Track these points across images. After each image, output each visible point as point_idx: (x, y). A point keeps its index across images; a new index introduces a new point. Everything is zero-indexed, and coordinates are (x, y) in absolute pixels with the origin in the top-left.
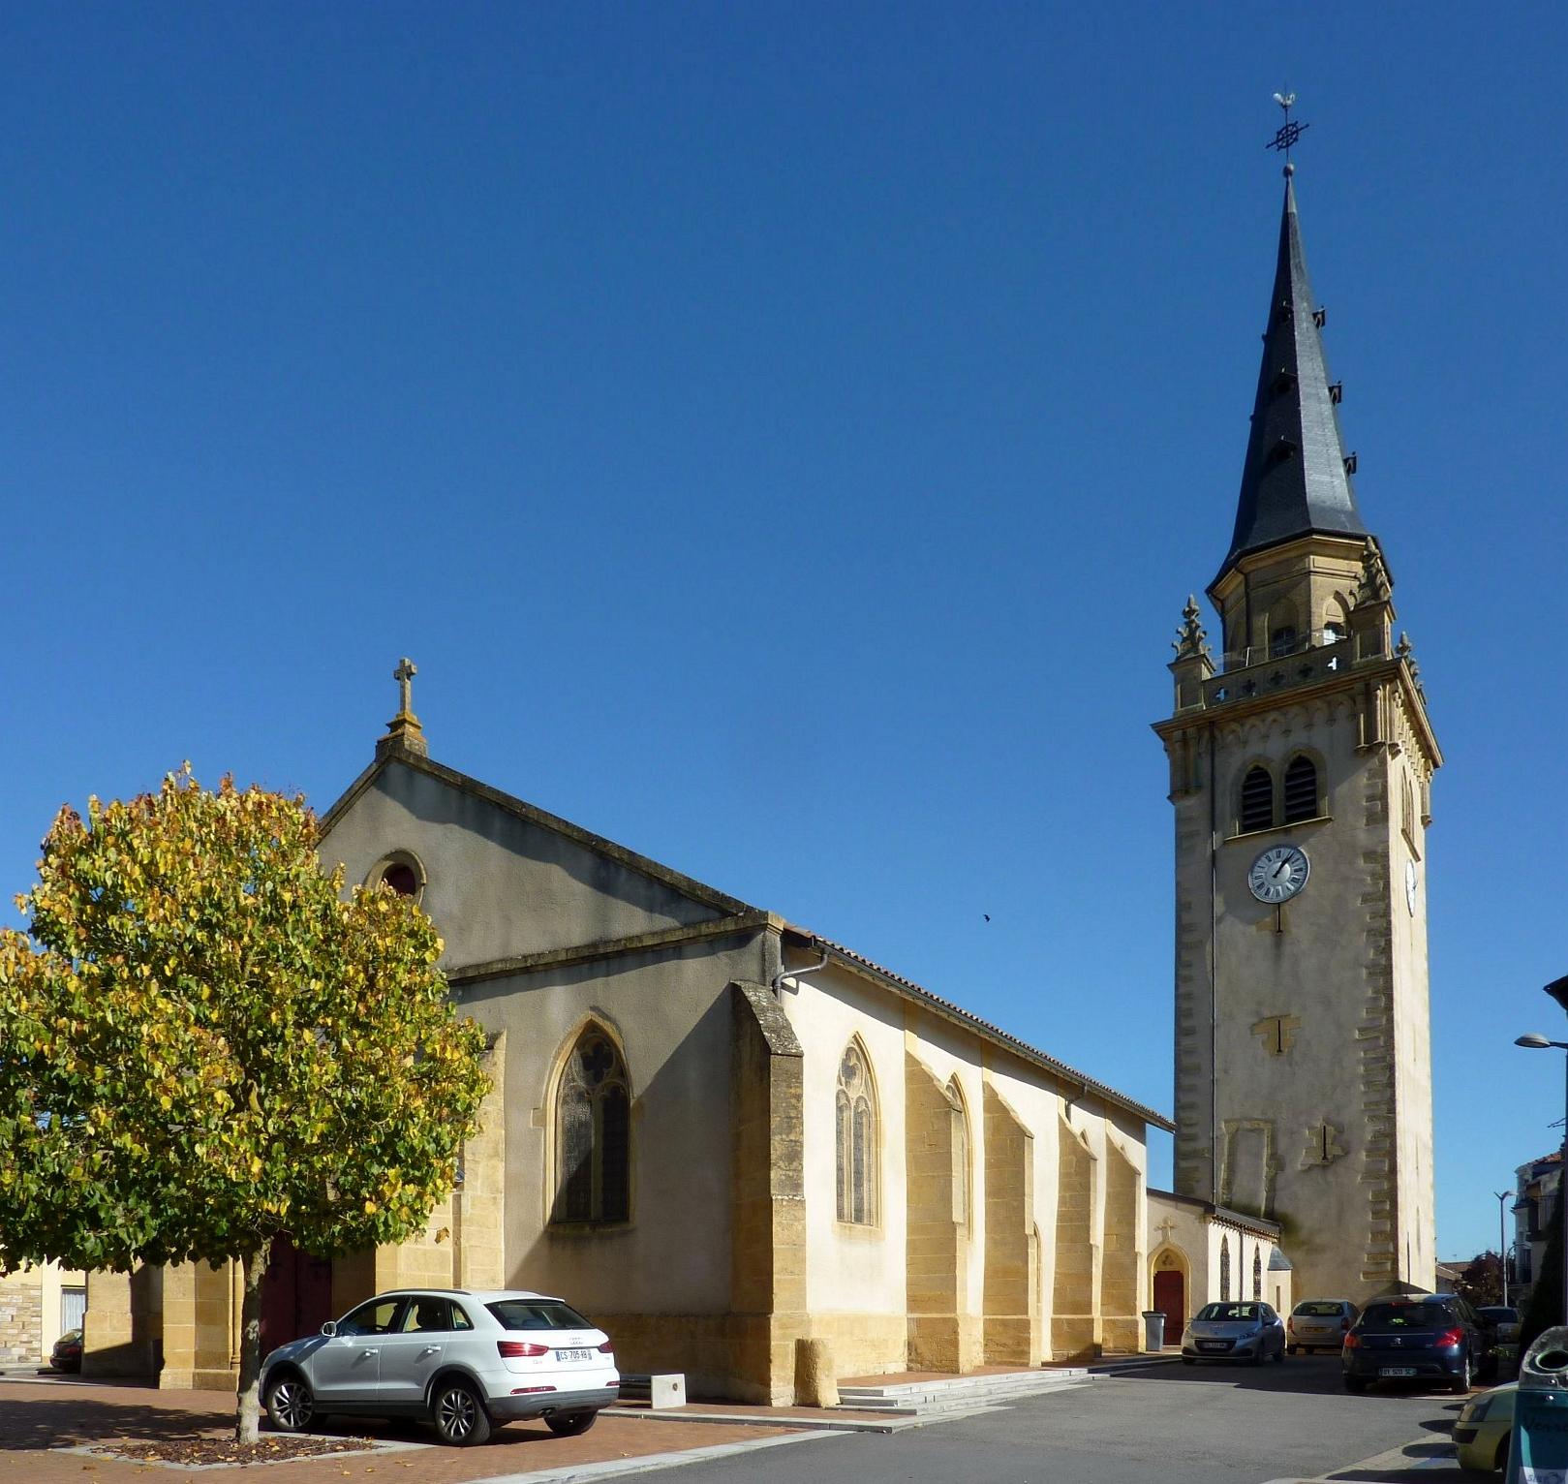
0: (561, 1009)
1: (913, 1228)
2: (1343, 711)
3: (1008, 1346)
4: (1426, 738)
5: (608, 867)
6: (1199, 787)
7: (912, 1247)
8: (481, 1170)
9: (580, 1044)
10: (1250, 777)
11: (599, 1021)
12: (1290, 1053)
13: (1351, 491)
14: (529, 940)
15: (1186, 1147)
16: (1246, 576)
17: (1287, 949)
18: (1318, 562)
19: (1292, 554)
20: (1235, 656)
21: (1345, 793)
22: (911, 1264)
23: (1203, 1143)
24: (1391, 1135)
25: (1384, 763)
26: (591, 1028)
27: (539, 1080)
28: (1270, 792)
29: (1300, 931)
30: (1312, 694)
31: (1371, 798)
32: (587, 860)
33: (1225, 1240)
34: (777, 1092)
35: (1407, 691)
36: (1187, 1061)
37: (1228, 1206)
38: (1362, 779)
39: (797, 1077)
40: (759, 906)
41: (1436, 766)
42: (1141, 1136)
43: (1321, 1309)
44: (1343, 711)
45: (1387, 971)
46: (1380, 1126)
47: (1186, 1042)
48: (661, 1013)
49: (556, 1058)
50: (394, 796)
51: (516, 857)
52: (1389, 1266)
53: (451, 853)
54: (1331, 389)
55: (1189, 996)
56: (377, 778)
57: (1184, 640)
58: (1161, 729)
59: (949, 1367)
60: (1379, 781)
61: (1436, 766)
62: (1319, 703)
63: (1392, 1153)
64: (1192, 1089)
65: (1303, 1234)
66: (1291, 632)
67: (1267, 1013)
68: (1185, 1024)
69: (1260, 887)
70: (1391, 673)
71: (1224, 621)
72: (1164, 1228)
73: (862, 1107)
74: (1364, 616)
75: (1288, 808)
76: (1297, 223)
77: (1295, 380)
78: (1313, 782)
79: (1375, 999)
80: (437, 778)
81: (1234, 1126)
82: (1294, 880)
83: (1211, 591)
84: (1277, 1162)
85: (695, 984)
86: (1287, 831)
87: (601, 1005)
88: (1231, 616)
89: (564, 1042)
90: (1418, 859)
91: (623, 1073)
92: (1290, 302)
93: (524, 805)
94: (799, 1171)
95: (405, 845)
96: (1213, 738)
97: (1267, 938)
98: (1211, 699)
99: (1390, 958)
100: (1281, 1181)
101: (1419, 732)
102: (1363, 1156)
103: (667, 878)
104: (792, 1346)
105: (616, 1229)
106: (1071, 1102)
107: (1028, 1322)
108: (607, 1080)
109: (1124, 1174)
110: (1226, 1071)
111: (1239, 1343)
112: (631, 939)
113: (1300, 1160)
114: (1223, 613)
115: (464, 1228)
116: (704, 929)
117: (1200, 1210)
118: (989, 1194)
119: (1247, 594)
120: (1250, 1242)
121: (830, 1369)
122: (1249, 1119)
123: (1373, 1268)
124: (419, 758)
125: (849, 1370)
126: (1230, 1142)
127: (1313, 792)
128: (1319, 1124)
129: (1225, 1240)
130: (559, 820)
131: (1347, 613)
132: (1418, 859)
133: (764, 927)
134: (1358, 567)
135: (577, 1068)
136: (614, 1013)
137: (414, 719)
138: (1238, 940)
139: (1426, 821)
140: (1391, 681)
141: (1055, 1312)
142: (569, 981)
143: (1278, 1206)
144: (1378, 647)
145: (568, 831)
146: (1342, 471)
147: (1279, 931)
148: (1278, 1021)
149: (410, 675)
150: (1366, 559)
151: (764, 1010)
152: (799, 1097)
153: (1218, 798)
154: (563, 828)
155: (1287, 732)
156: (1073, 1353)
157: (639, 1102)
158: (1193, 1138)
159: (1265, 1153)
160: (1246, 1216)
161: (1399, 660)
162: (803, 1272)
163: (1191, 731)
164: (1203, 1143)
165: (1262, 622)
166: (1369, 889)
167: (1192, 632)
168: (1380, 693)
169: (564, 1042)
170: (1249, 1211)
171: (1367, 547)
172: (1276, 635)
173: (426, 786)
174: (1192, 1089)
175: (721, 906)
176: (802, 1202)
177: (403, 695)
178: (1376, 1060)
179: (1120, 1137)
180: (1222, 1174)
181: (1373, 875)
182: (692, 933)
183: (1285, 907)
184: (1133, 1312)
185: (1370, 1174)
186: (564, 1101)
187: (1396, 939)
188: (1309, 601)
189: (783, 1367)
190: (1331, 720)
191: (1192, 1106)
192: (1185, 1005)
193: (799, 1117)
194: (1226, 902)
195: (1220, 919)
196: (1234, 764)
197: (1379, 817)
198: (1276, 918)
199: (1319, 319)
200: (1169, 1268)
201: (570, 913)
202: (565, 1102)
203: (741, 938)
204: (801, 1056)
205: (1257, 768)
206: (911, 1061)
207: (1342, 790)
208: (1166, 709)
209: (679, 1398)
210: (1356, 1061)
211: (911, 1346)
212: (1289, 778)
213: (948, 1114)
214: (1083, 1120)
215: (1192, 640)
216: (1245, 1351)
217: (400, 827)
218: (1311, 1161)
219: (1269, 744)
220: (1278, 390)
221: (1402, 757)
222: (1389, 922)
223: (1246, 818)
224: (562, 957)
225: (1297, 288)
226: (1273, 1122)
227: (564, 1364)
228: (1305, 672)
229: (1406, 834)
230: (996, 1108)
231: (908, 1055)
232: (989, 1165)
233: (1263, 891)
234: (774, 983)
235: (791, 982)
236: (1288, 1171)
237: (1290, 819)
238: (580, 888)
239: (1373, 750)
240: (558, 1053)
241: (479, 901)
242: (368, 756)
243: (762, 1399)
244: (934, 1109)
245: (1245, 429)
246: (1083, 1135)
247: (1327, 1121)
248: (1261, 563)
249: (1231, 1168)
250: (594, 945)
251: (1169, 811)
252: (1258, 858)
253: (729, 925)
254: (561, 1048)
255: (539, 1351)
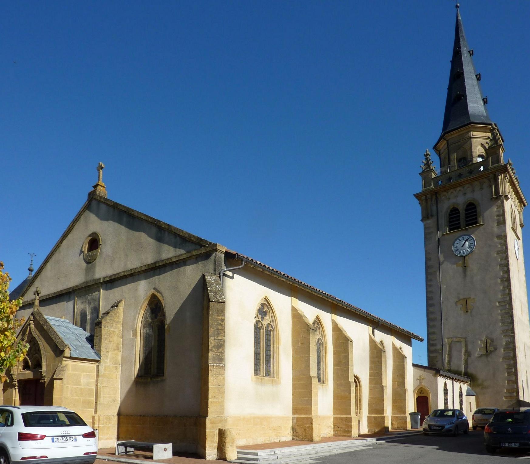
0: (142, 289)
1: (295, 379)
2: (486, 185)
3: (343, 428)
4: (519, 195)
5: (162, 232)
6: (432, 216)
7: (294, 387)
8: (109, 355)
9: (150, 304)
10: (451, 211)
11: (156, 293)
12: (471, 312)
13: (486, 109)
14: (134, 262)
15: (432, 348)
16: (447, 141)
17: (468, 273)
18: (474, 134)
19: (465, 131)
20: (444, 169)
21: (488, 215)
22: (294, 394)
23: (439, 347)
24: (514, 342)
25: (503, 202)
26: (153, 297)
27: (134, 319)
28: (459, 216)
29: (473, 266)
30: (475, 179)
31: (498, 216)
32: (154, 230)
33: (445, 384)
34: (213, 319)
35: (510, 177)
36: (431, 316)
37: (449, 371)
38: (495, 209)
39: (222, 312)
40: (213, 242)
41: (524, 206)
42: (409, 343)
43: (486, 412)
44: (486, 185)
45: (508, 280)
46: (508, 339)
47: (431, 309)
48: (176, 289)
49: (140, 309)
50: (93, 213)
51: (130, 231)
52: (515, 394)
53: (110, 232)
54: (476, 76)
55: (431, 292)
56: (88, 207)
57: (425, 165)
58: (417, 196)
59: (309, 439)
60: (501, 209)
61: (524, 206)
62: (477, 183)
63: (514, 350)
64: (434, 326)
65: (480, 382)
66: (465, 159)
67: (461, 297)
68: (430, 302)
69: (457, 250)
70: (504, 170)
71: (440, 158)
72: (419, 379)
73: (270, 328)
74: (492, 151)
75: (467, 221)
76: (461, 23)
77: (463, 73)
78: (476, 211)
79: (504, 290)
80: (106, 204)
81: (450, 340)
82: (470, 247)
83: (435, 148)
84: (468, 354)
85: (190, 275)
86: (467, 230)
87: (156, 287)
88: (442, 156)
89: (144, 303)
90: (519, 239)
91: (164, 315)
92: (460, 48)
93: (133, 210)
94: (223, 353)
95: (95, 231)
96: (437, 198)
97: (460, 269)
98: (436, 184)
99: (509, 275)
100: (470, 361)
101: (517, 193)
102: (502, 350)
103: (181, 234)
104: (217, 432)
105: (159, 379)
106: (374, 328)
107: (351, 418)
108: (158, 317)
109: (400, 358)
110: (446, 320)
111: (447, 427)
112: (167, 259)
113: (477, 353)
114: (439, 155)
115: (100, 379)
116: (194, 253)
117: (434, 372)
118: (335, 365)
119: (448, 147)
120: (457, 385)
121: (233, 441)
122: (456, 338)
123: (508, 395)
124: (101, 197)
125: (242, 442)
126: (449, 346)
127: (476, 215)
128: (484, 339)
129: (445, 384)
130: (144, 215)
131: (486, 150)
132: (519, 239)
133: (216, 250)
134: (489, 135)
135: (148, 314)
136: (161, 289)
137: (103, 184)
138: (449, 271)
139: (521, 226)
140: (504, 173)
141: (369, 413)
142: (146, 278)
143: (469, 371)
144: (498, 161)
145: (147, 219)
146: (482, 103)
147: (465, 267)
148: (466, 300)
149: (102, 168)
150: (492, 131)
151: (212, 284)
152: (223, 320)
153: (440, 220)
154: (145, 218)
155: (465, 194)
156: (376, 430)
157: (169, 327)
158: (435, 345)
159: (463, 350)
160: (455, 374)
161: (506, 165)
162: (223, 398)
163: (429, 196)
164: (439, 347)
165: (454, 156)
166: (500, 249)
167: (428, 162)
168: (500, 177)
169: (144, 303)
170: (458, 373)
171: (492, 127)
172: (459, 161)
173: (103, 207)
174: (434, 326)
175: (199, 243)
176: (223, 367)
177: (99, 176)
178: (506, 313)
179: (399, 343)
180: (446, 359)
181: (501, 244)
182: (189, 255)
183: (467, 258)
184: (404, 412)
185: (506, 358)
186: (144, 326)
187: (511, 268)
188: (471, 147)
189: (212, 441)
190: (482, 189)
191: (434, 333)
192: (430, 295)
193: (223, 329)
194: (445, 257)
195: (442, 263)
196: (445, 206)
197: (502, 222)
198: (463, 262)
199: (471, 53)
200: (422, 395)
201: (147, 250)
202: (144, 328)
203: (207, 256)
204: (224, 303)
205: (454, 208)
206: (294, 309)
207: (487, 214)
208: (419, 188)
209: (169, 454)
210: (498, 314)
211: (294, 429)
212: (466, 210)
213: (308, 331)
214: (379, 336)
215: (428, 164)
216: (449, 430)
217: (94, 224)
218: (482, 353)
219: (458, 199)
220: (457, 77)
221: (510, 200)
222: (508, 261)
223: (450, 226)
224: (143, 269)
225: (462, 43)
226: (466, 338)
227: (56, 444)
228: (471, 172)
229: (514, 229)
230: (337, 329)
231: (293, 307)
232: (335, 353)
233: (458, 252)
234: (220, 274)
235: (230, 274)
236: (472, 357)
237: (467, 225)
238: (151, 241)
239: (498, 198)
240: (141, 308)
241: (123, 250)
242: (84, 200)
243: (201, 456)
244: (303, 330)
245: (446, 92)
246: (400, 348)
247: (487, 337)
248: (454, 135)
249: (450, 357)
250: (155, 263)
251: (422, 225)
252: (456, 240)
253: (203, 251)
254: (142, 305)
255: (43, 437)
